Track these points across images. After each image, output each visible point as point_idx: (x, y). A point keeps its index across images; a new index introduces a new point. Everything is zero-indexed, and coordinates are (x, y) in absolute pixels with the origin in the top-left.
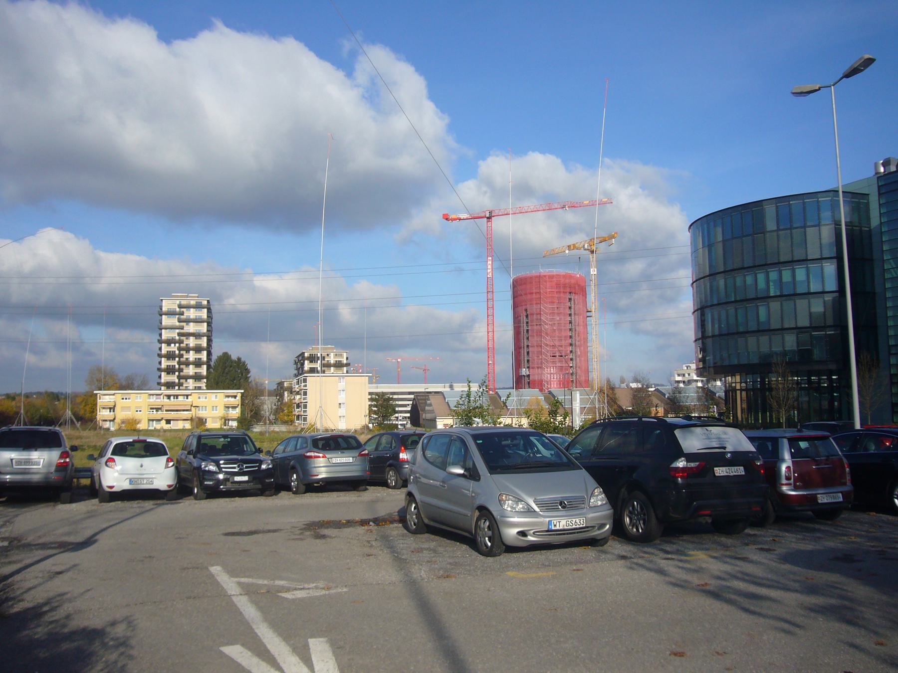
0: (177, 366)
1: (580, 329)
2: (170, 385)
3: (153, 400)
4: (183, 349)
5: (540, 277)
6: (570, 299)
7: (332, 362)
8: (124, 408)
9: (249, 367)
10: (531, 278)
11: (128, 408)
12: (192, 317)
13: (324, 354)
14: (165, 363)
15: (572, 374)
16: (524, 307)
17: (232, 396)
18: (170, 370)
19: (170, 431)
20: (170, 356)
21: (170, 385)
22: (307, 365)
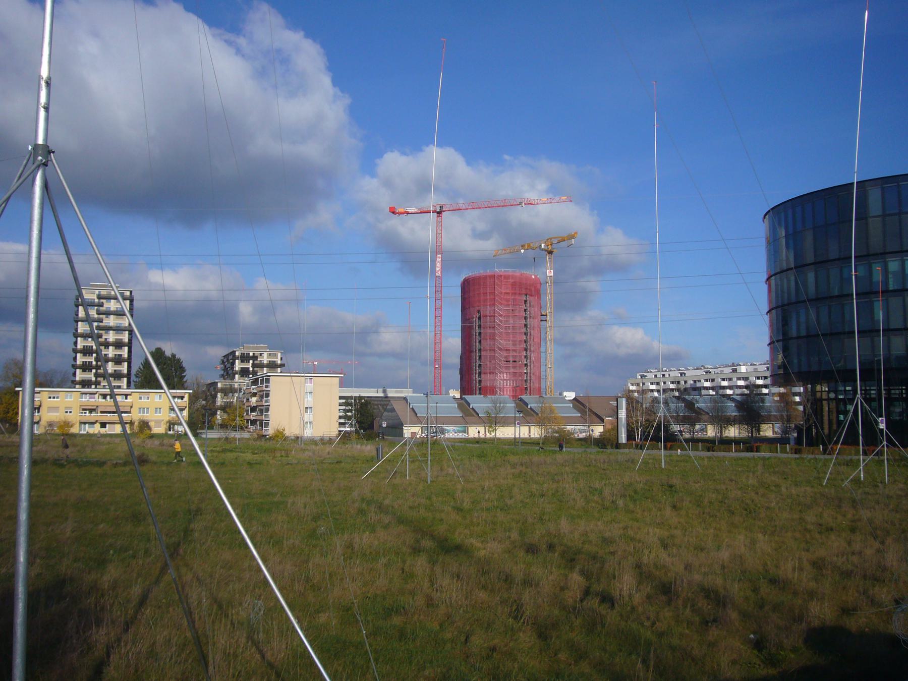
0: (251, 369)
1: (534, 333)
2: (85, 384)
3: (85, 399)
4: (101, 344)
5: (493, 277)
6: (526, 301)
7: (265, 362)
8: (55, 409)
9: (184, 365)
10: (485, 277)
11: (55, 409)
12: (112, 309)
13: (257, 353)
14: (80, 359)
15: (526, 381)
16: (477, 309)
17: (178, 397)
18: (86, 367)
19: (492, 440)
20: (87, 351)
21: (85, 384)
22: (238, 365)
